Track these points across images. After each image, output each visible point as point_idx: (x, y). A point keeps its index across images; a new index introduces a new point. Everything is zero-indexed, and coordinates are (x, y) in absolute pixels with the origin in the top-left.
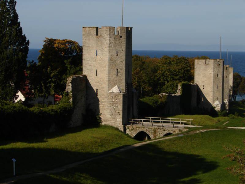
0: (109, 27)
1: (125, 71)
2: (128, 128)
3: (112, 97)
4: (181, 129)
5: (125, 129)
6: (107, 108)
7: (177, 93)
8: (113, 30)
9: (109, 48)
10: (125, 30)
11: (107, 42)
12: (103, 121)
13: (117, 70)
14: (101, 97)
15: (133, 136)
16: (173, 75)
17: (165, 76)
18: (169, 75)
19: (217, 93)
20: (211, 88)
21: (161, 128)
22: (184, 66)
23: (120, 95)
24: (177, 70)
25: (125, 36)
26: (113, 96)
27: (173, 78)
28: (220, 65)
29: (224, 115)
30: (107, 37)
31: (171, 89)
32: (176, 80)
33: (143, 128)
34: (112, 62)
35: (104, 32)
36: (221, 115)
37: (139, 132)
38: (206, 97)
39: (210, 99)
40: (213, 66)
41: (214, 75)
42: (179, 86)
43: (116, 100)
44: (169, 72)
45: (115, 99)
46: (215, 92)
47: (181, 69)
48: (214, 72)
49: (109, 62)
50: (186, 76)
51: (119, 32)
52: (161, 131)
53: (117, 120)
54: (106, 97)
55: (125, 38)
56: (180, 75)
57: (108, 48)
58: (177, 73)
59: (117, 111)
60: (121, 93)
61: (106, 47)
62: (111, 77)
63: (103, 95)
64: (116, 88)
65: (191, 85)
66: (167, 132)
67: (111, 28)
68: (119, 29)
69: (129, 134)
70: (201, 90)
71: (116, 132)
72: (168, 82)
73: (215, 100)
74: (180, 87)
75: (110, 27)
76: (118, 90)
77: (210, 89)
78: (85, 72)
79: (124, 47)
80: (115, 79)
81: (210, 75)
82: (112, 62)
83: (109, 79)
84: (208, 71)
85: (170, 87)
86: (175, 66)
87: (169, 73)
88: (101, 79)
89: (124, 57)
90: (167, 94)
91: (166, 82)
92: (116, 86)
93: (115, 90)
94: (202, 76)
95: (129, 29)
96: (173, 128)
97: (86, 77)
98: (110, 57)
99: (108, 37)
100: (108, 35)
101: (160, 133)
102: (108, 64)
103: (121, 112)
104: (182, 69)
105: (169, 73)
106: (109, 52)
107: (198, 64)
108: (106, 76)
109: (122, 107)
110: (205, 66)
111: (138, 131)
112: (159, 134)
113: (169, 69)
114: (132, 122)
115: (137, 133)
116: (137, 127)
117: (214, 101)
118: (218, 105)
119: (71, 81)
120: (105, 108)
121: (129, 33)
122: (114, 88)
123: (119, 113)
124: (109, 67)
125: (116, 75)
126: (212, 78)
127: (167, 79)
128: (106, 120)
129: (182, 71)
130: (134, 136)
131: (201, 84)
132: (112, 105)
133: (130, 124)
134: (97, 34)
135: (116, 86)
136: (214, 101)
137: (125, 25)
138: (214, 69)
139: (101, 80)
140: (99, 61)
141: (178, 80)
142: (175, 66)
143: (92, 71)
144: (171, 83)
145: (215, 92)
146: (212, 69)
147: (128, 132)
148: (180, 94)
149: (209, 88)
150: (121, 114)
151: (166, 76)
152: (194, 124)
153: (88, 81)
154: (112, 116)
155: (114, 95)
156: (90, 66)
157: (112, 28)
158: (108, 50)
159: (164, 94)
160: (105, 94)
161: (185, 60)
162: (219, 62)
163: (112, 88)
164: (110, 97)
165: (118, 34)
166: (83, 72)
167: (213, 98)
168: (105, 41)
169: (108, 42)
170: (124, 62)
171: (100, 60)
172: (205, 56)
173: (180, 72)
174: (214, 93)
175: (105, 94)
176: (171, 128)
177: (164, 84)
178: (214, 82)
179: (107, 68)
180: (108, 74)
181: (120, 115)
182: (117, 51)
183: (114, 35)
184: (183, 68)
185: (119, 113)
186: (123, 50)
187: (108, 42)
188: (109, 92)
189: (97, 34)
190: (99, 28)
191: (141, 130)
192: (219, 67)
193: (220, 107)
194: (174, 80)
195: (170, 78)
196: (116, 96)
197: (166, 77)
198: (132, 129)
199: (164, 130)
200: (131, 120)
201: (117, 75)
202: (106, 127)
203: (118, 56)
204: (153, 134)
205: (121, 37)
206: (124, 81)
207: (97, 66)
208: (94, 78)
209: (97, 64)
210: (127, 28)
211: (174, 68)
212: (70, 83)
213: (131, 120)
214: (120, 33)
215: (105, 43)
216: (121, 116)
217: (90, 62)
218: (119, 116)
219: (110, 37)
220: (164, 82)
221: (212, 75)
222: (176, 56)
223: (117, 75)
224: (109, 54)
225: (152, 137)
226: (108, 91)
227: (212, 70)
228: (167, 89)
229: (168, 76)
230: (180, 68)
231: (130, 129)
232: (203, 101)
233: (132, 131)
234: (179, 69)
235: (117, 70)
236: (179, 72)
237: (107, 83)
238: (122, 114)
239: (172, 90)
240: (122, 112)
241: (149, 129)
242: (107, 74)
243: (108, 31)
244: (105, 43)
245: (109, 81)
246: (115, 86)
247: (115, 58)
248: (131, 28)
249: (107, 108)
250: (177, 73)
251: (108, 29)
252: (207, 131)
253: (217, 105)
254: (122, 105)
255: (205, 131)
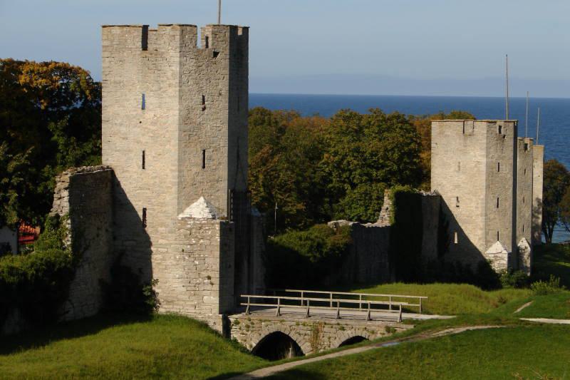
0: (180, 26)
1: (226, 155)
2: (237, 323)
3: (189, 232)
4: (391, 325)
5: (227, 326)
6: (174, 263)
7: (379, 221)
8: (192, 35)
9: (180, 87)
10: (228, 34)
11: (173, 68)
12: (161, 300)
13: (204, 151)
14: (157, 231)
15: (251, 346)
16: (370, 166)
17: (344, 171)
18: (356, 166)
19: (497, 220)
20: (479, 205)
21: (334, 322)
22: (401, 139)
23: (213, 224)
24: (381, 154)
25: (228, 52)
26: (190, 229)
27: (367, 174)
28: (504, 137)
29: (517, 283)
30: (174, 55)
31: (363, 208)
32: (378, 181)
33: (281, 321)
34: (188, 127)
35: (166, 38)
36: (508, 282)
37: (267, 333)
38: (466, 232)
39: (476, 237)
40: (485, 141)
41: (488, 166)
42: (386, 198)
43: (202, 241)
44: (355, 158)
45: (196, 237)
46: (492, 216)
47: (393, 149)
48: (487, 156)
49: (180, 130)
50: (406, 169)
51: (210, 39)
52: (334, 330)
53: (205, 297)
54: (169, 232)
55: (228, 57)
56: (387, 167)
57: (178, 89)
58: (381, 161)
59: (205, 274)
60: (214, 218)
61: (170, 85)
62: (185, 173)
63: (162, 225)
64: (201, 206)
65: (421, 195)
66: (349, 334)
67: (187, 30)
68: (209, 33)
69: (239, 341)
70: (450, 212)
71: (202, 334)
72: (354, 186)
73: (492, 240)
74: (388, 203)
75: (183, 25)
76: (207, 210)
77: (476, 208)
78: (110, 157)
79: (224, 85)
80: (199, 178)
81: (476, 166)
82: (188, 127)
83: (179, 177)
84: (472, 153)
85: (362, 202)
86: (375, 141)
87: (355, 162)
88: (156, 177)
89: (224, 115)
90: (351, 224)
91: (347, 186)
92: (202, 199)
93: (199, 210)
94: (452, 169)
95: (240, 33)
96: (369, 323)
97: (112, 172)
98: (185, 112)
99: (178, 54)
100: (178, 50)
101: (329, 338)
102: (177, 134)
103: (216, 276)
104: (396, 150)
105: (355, 162)
106: (180, 98)
107: (441, 133)
108: (172, 171)
109: (218, 260)
110: (462, 141)
111: (265, 333)
112: (326, 339)
113: (357, 150)
114: (248, 304)
115: (263, 336)
116: (261, 321)
117: (489, 241)
118: (500, 255)
119: (67, 185)
120: (168, 262)
121: (238, 42)
122: (195, 204)
123: (209, 278)
124: (179, 145)
125: (202, 165)
126: (484, 177)
127: (351, 178)
128: (170, 299)
129: (396, 156)
130: (254, 345)
131: (449, 194)
132: (190, 254)
133: (241, 310)
134: (145, 47)
135: (202, 199)
136: (488, 244)
137: (228, 20)
138: (488, 148)
139: (157, 180)
140: (149, 127)
141: (383, 181)
142: (375, 141)
143: (132, 155)
144: (362, 189)
145: (492, 216)
146: (481, 149)
147: (235, 334)
148: (390, 221)
149: (473, 205)
150: (216, 280)
151: (349, 170)
152: (430, 311)
153: (118, 184)
154: (189, 288)
155: (194, 224)
156: (124, 139)
157: (188, 28)
158: (177, 93)
159: (342, 222)
160: (169, 222)
161: (404, 122)
162: (502, 129)
163: (188, 205)
164: (182, 231)
165: (207, 46)
166: (104, 158)
167: (487, 234)
168: (167, 68)
169: (176, 68)
170: (225, 129)
171: (154, 123)
172: (462, 112)
173: (388, 159)
174: (487, 220)
175: (169, 222)
176: (363, 323)
177: (342, 193)
178: (488, 187)
179: (172, 148)
180: (176, 163)
181: (212, 284)
182: (203, 97)
183: (195, 50)
184: (396, 146)
185: (209, 278)
186: (220, 94)
187: (178, 69)
188: (181, 216)
189: (145, 47)
190: (149, 28)
191: (273, 328)
192: (503, 145)
193: (505, 262)
194: (371, 180)
195: (360, 175)
196: (200, 228)
197: (348, 173)
198: (248, 326)
199: (343, 329)
200: (245, 300)
201: (204, 167)
202: (172, 318)
203: (206, 111)
204: (310, 341)
205: (216, 54)
206: (224, 185)
207: (144, 139)
208: (135, 176)
209: (143, 135)
210: (233, 29)
211: (370, 145)
212: (66, 189)
213: (245, 300)
214: (213, 44)
215: (169, 74)
216: (217, 287)
217: (123, 129)
218: (209, 287)
219: (183, 54)
220: (343, 188)
221: (483, 168)
222: (377, 112)
223: (204, 167)
224: (180, 103)
225: (306, 347)
226: (178, 214)
227: (484, 153)
228: (350, 208)
229: (355, 170)
230: (389, 147)
231: (243, 324)
232: (456, 242)
233: (248, 331)
234: (386, 150)
235: (204, 154)
236: (386, 158)
237: (175, 189)
238: (218, 283)
239: (366, 210)
240: (218, 276)
241: (298, 324)
242: (173, 165)
243: (178, 37)
244: (169, 74)
245: (180, 183)
246: (197, 199)
247: (197, 116)
248: (246, 30)
249: (174, 263)
250: (381, 161)
251: (178, 33)
252: (468, 330)
253: (497, 254)
254: (217, 253)
255: (462, 329)
